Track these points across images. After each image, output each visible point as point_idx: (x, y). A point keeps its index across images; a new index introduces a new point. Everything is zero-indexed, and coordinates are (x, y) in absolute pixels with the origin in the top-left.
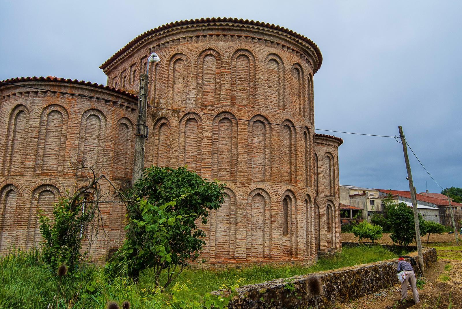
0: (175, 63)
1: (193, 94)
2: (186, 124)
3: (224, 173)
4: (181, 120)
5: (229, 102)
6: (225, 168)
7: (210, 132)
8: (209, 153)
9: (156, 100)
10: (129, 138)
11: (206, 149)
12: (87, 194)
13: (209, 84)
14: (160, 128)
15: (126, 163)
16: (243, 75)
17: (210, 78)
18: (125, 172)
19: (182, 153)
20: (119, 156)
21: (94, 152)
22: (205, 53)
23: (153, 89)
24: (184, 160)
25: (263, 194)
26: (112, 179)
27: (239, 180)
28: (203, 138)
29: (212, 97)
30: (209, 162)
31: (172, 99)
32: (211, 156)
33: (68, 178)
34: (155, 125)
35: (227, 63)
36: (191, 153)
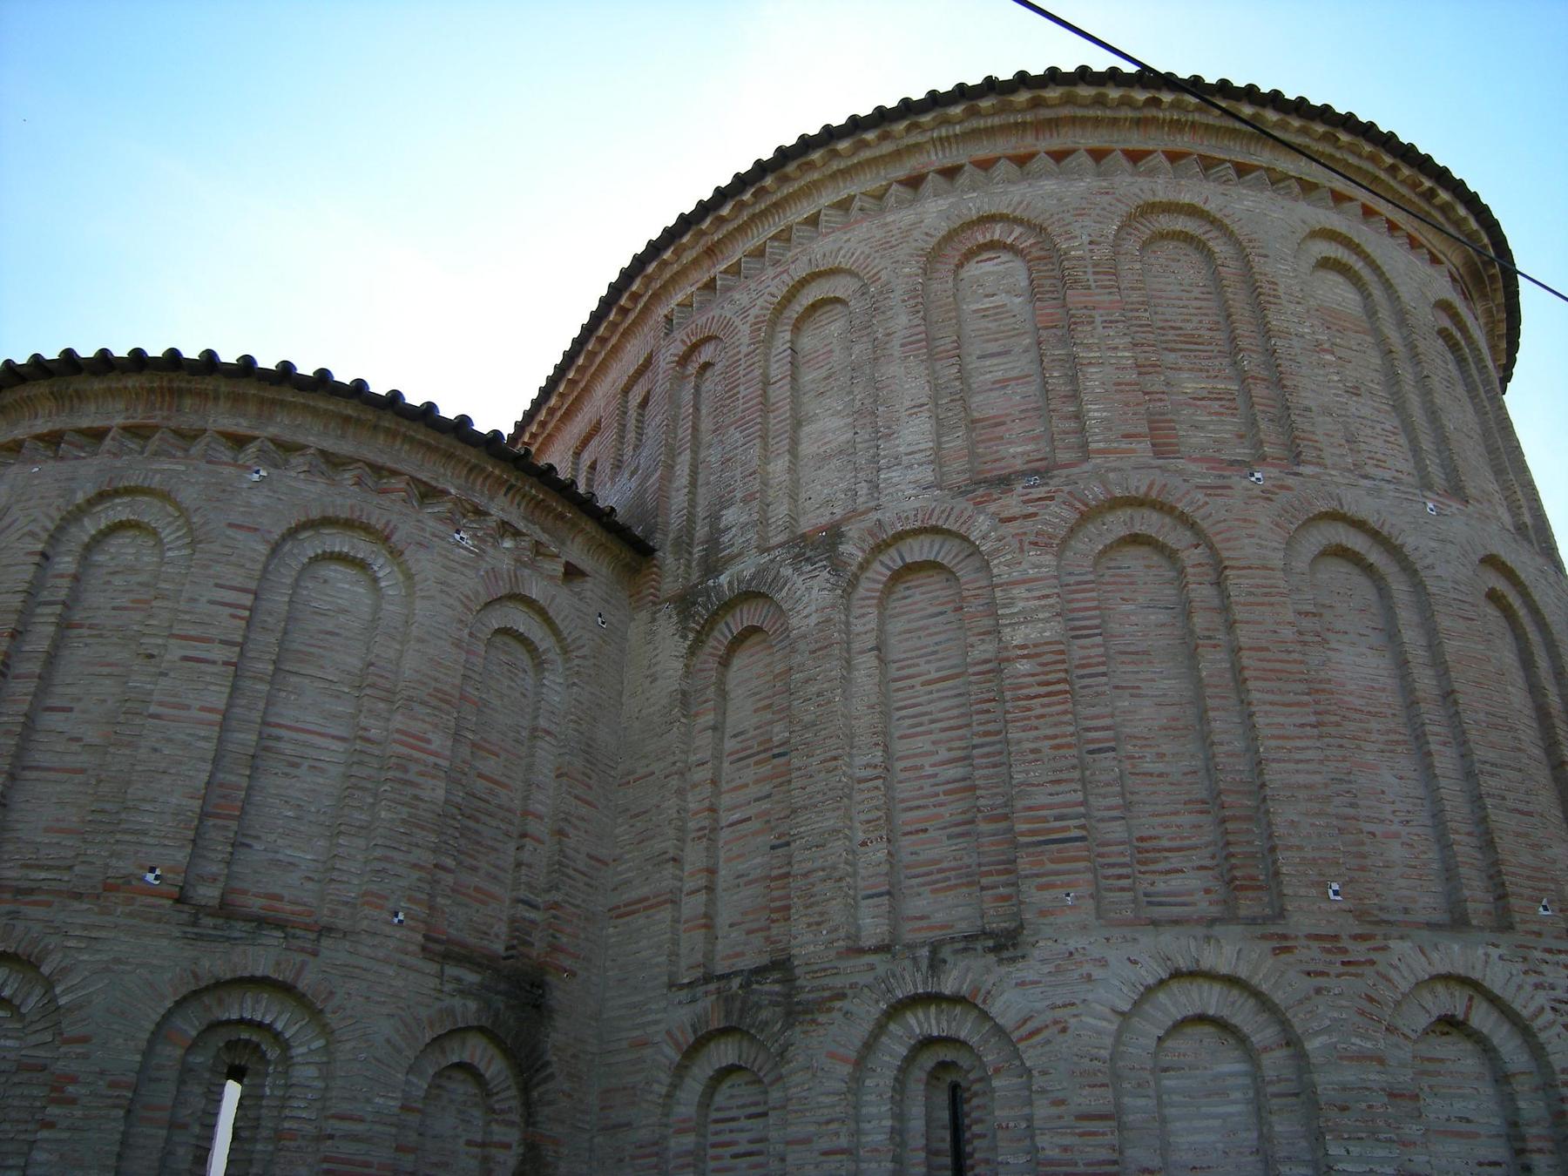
0: (797, 328)
1: (915, 433)
2: (882, 603)
3: (1176, 882)
4: (853, 583)
5: (1143, 447)
6: (1179, 849)
7: (1046, 620)
8: (1058, 747)
9: (701, 532)
10: (542, 723)
11: (1034, 722)
12: (245, 1036)
13: (1003, 383)
14: (725, 662)
15: (519, 865)
16: (1189, 326)
17: (1007, 353)
18: (513, 920)
19: (869, 772)
20: (483, 818)
21: (322, 771)
22: (964, 244)
23: (685, 480)
24: (889, 819)
25: (1482, 1018)
26: (424, 949)
27: (1301, 922)
28: (1008, 660)
29: (1033, 439)
30: (1066, 805)
31: (793, 497)
32: (1074, 767)
33: (130, 915)
34: (692, 651)
35: (1095, 266)
36: (929, 771)
